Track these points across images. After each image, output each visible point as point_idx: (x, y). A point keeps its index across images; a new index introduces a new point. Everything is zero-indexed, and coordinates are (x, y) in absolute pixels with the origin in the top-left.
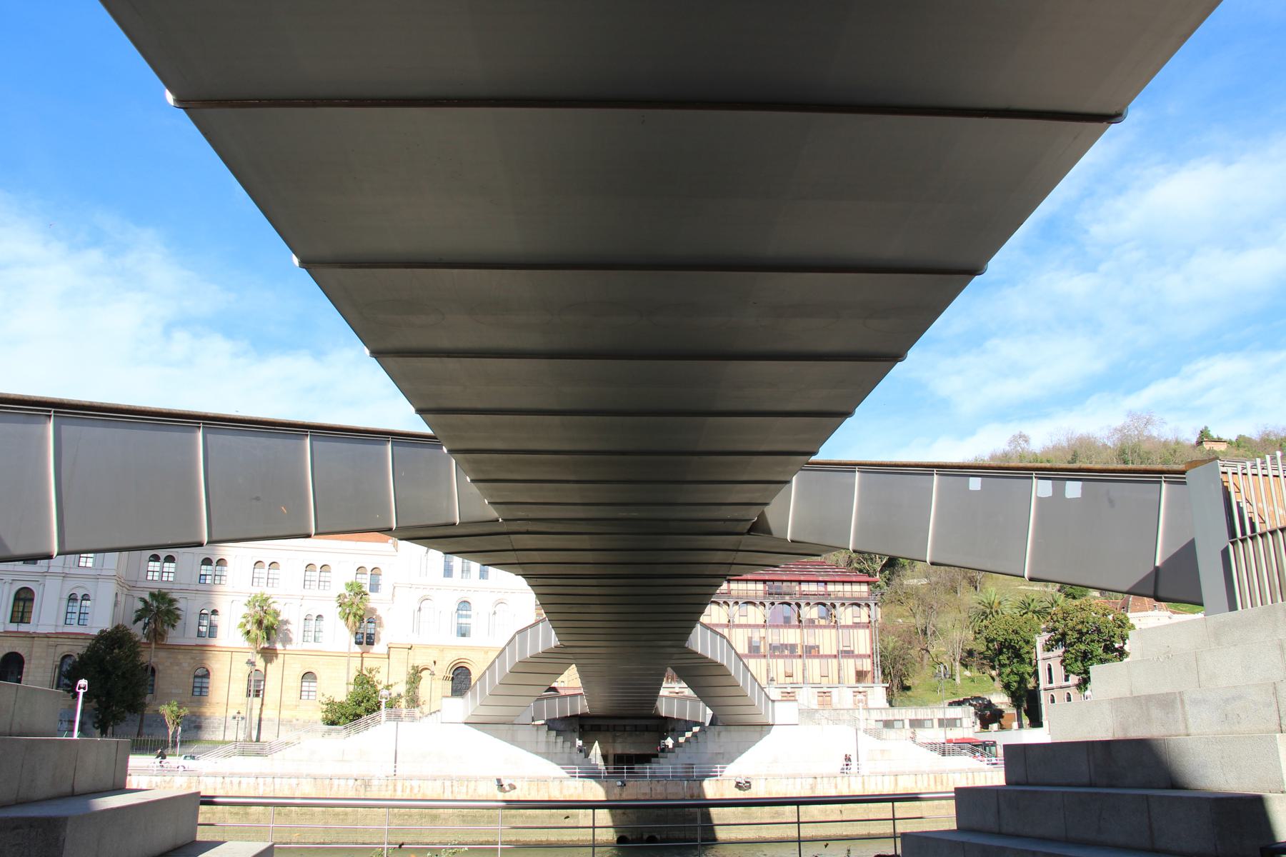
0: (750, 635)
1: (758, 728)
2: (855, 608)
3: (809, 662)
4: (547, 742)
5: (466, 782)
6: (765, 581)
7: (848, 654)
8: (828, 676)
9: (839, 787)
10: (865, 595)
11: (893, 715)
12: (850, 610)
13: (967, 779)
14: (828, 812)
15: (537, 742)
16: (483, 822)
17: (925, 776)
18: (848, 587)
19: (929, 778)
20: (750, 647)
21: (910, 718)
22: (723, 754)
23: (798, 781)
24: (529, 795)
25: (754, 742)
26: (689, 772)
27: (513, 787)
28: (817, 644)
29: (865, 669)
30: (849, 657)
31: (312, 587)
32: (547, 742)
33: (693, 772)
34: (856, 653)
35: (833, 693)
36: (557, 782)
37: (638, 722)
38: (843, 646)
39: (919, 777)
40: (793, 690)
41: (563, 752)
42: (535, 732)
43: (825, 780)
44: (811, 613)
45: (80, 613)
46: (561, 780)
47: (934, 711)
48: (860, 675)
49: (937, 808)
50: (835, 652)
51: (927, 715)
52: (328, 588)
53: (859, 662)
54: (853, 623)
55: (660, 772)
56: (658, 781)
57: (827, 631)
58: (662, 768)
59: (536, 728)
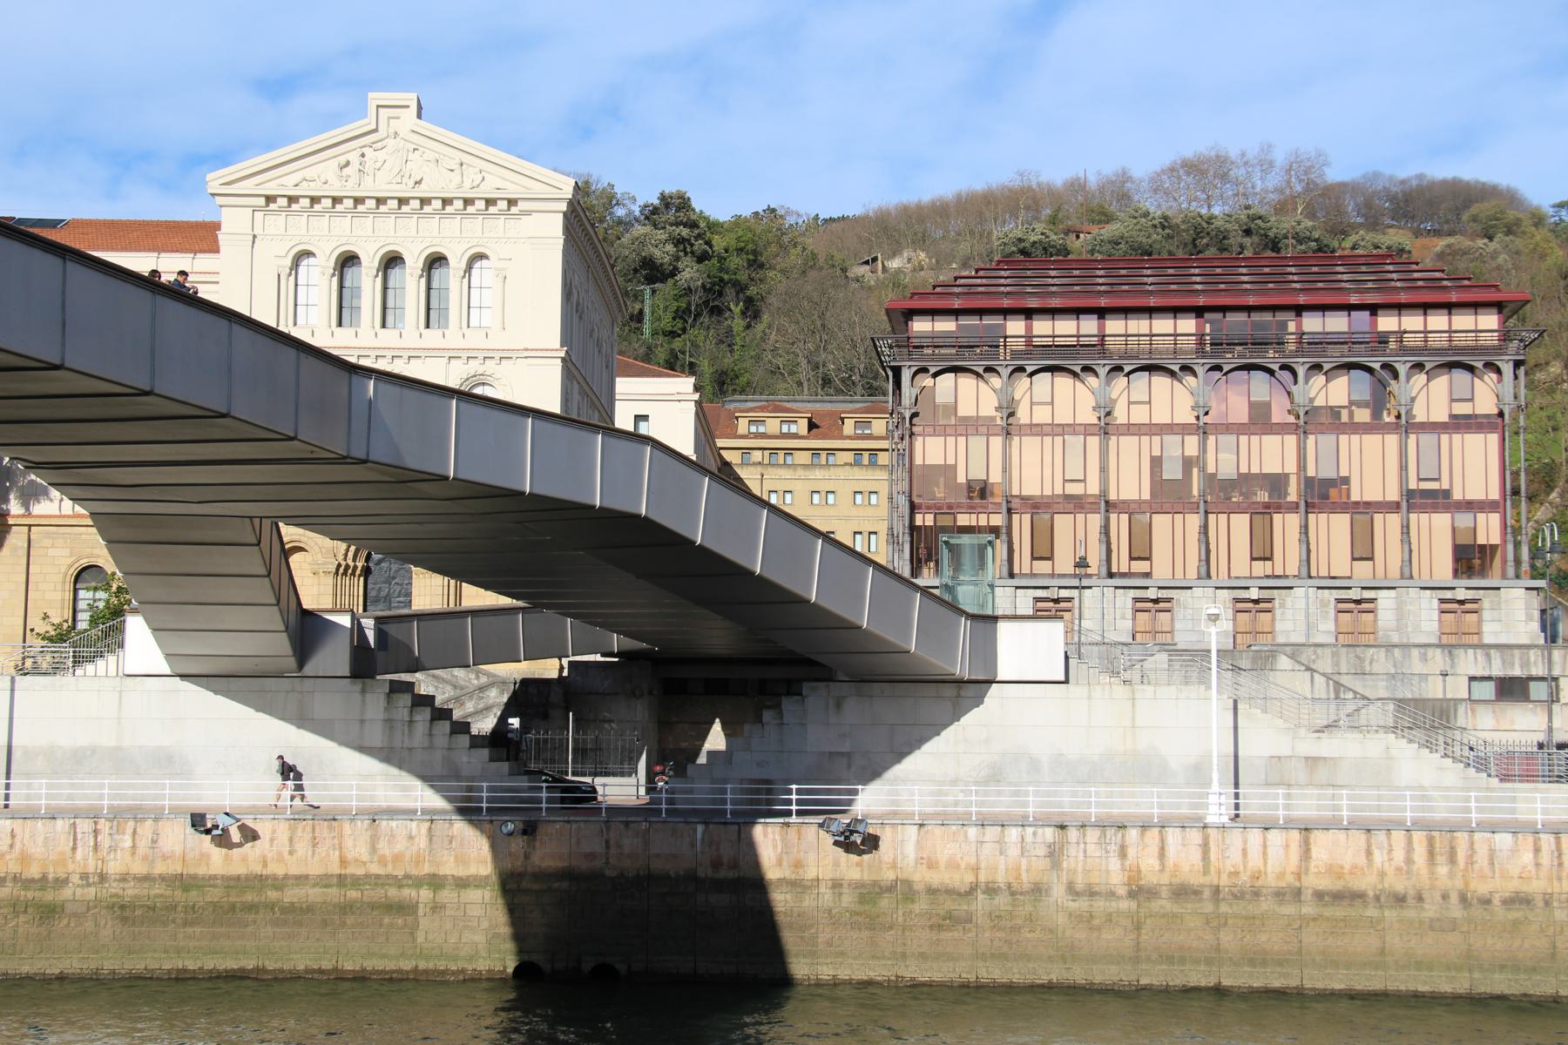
0: (1157, 453)
1: (949, 691)
2: (1461, 376)
3: (1318, 521)
4: (389, 722)
5: (131, 824)
6: (1199, 312)
7: (1436, 500)
8: (1371, 559)
9: (1131, 852)
10: (1492, 339)
12: (1442, 382)
13: (1537, 850)
14: (1096, 922)
15: (362, 721)
16: (174, 921)
17: (1398, 837)
18: (1438, 321)
19: (1410, 842)
20: (1158, 484)
22: (848, 755)
23: (1013, 833)
24: (291, 853)
25: (936, 728)
27: (250, 835)
28: (1343, 473)
29: (1481, 540)
30: (1435, 509)
32: (386, 721)
33: (724, 801)
34: (1457, 495)
35: (1381, 604)
36: (362, 824)
38: (1420, 480)
39: (1380, 837)
40: (1266, 594)
41: (431, 747)
42: (357, 696)
43: (1092, 835)
44: (1337, 391)
46: (431, 815)
47: (1425, 654)
48: (1470, 559)
49: (1432, 928)
50: (1393, 495)
53: (1464, 520)
54: (1452, 416)
55: (687, 801)
56: (627, 824)
57: (1372, 441)
58: (691, 791)
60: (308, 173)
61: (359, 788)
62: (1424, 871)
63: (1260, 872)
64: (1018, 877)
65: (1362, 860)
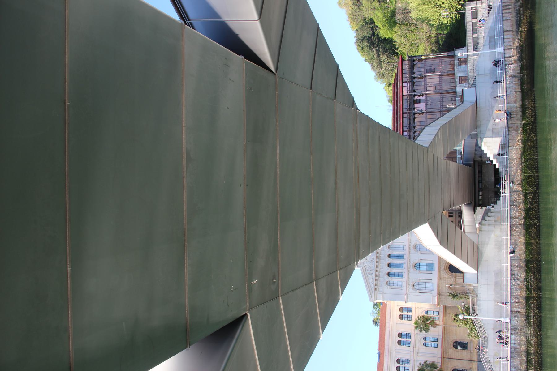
4: (489, 225)
11: (470, 43)
15: (488, 231)
17: (504, 15)
21: (471, 19)
23: (509, 123)
26: (504, 147)
31: (408, 369)
33: (504, 144)
37: (477, 176)
41: (494, 216)
45: (432, 341)
51: (470, 25)
52: (410, 316)
55: (504, 162)
59: (481, 232)
60: (371, 281)
61: (499, 36)
62: (511, 10)
63: (513, 39)
64: (517, 84)
65: (509, 21)
